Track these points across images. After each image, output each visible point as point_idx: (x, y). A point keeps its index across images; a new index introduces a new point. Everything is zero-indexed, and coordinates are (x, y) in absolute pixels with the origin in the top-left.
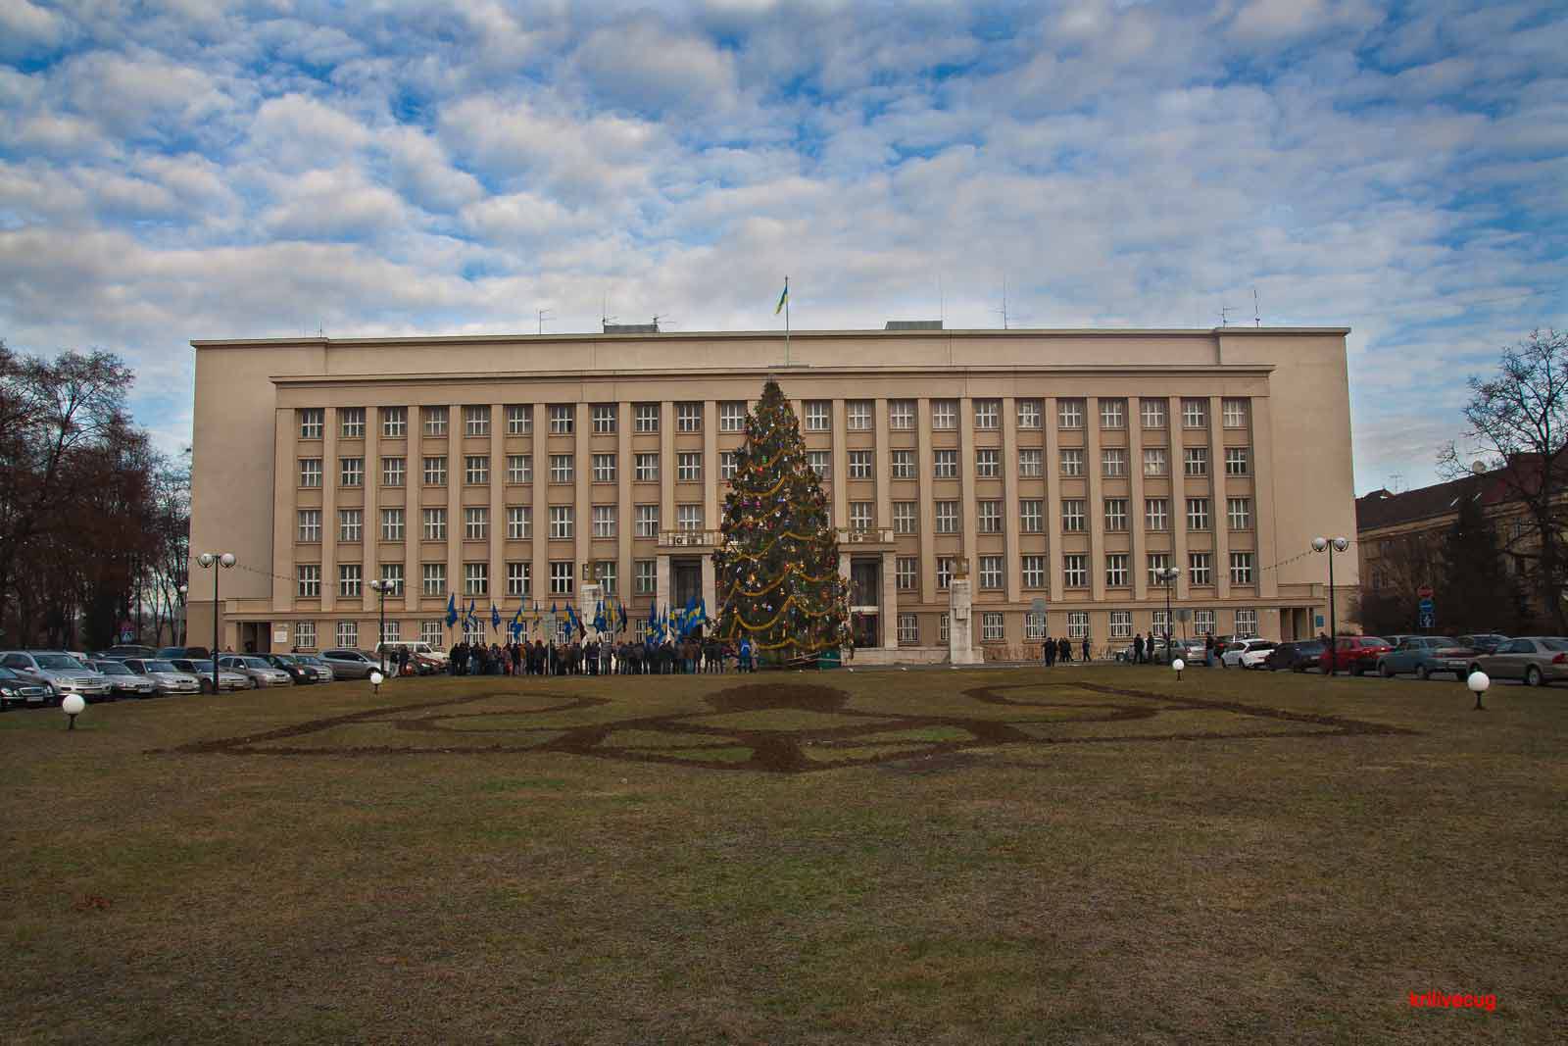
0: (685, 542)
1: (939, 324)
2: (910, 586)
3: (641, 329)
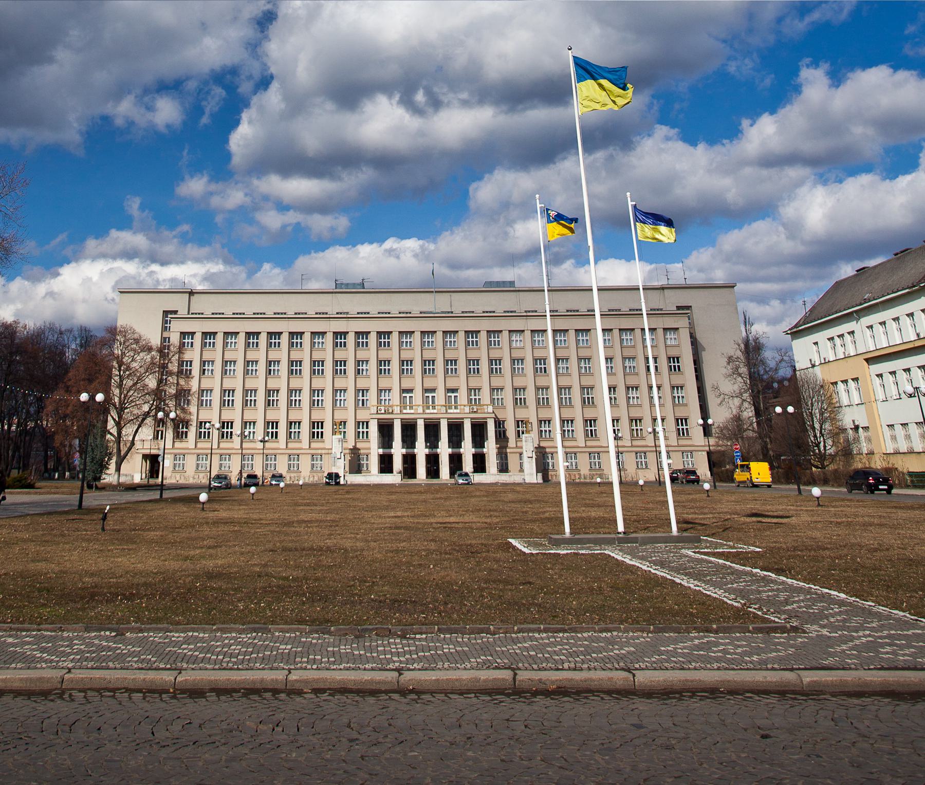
0: (383, 411)
1: (512, 283)
2: (501, 437)
3: (354, 285)
